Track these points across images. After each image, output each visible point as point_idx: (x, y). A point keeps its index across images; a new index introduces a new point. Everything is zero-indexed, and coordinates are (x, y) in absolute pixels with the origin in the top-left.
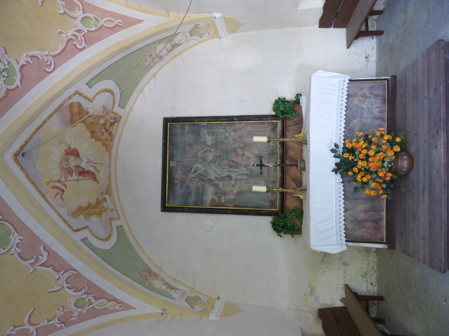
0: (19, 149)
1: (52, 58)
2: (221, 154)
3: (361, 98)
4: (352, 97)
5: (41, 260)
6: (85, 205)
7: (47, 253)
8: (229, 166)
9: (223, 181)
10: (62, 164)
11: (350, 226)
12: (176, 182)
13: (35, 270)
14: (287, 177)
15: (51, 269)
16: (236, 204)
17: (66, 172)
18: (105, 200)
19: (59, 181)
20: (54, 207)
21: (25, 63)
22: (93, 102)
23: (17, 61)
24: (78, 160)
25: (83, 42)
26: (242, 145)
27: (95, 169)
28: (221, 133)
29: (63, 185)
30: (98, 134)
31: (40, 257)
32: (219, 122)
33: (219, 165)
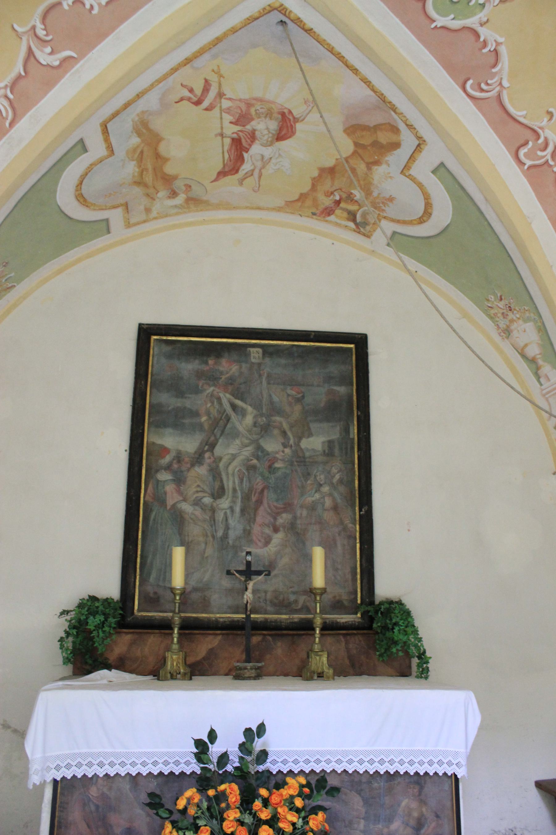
0: (296, 15)
1: (496, 95)
2: (279, 474)
3: (415, 814)
4: (418, 793)
5: (42, 51)
6: (162, 149)
7: (57, 63)
8: (247, 491)
9: (211, 478)
10: (259, 103)
11: (94, 792)
12: (211, 362)
13: (19, 36)
14: (220, 637)
15: (20, 71)
16: (151, 509)
17: (242, 111)
18: (173, 194)
19: (221, 95)
20: (160, 82)
21: (482, 39)
22: (402, 176)
23: (485, 23)
24: (268, 138)
25: (534, 160)
26: (299, 526)
27: (246, 173)
28: (329, 472)
29: (211, 104)
30: (327, 185)
31: (49, 50)
32: (356, 469)
33: (251, 468)
